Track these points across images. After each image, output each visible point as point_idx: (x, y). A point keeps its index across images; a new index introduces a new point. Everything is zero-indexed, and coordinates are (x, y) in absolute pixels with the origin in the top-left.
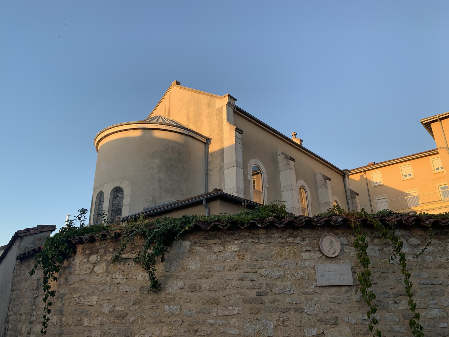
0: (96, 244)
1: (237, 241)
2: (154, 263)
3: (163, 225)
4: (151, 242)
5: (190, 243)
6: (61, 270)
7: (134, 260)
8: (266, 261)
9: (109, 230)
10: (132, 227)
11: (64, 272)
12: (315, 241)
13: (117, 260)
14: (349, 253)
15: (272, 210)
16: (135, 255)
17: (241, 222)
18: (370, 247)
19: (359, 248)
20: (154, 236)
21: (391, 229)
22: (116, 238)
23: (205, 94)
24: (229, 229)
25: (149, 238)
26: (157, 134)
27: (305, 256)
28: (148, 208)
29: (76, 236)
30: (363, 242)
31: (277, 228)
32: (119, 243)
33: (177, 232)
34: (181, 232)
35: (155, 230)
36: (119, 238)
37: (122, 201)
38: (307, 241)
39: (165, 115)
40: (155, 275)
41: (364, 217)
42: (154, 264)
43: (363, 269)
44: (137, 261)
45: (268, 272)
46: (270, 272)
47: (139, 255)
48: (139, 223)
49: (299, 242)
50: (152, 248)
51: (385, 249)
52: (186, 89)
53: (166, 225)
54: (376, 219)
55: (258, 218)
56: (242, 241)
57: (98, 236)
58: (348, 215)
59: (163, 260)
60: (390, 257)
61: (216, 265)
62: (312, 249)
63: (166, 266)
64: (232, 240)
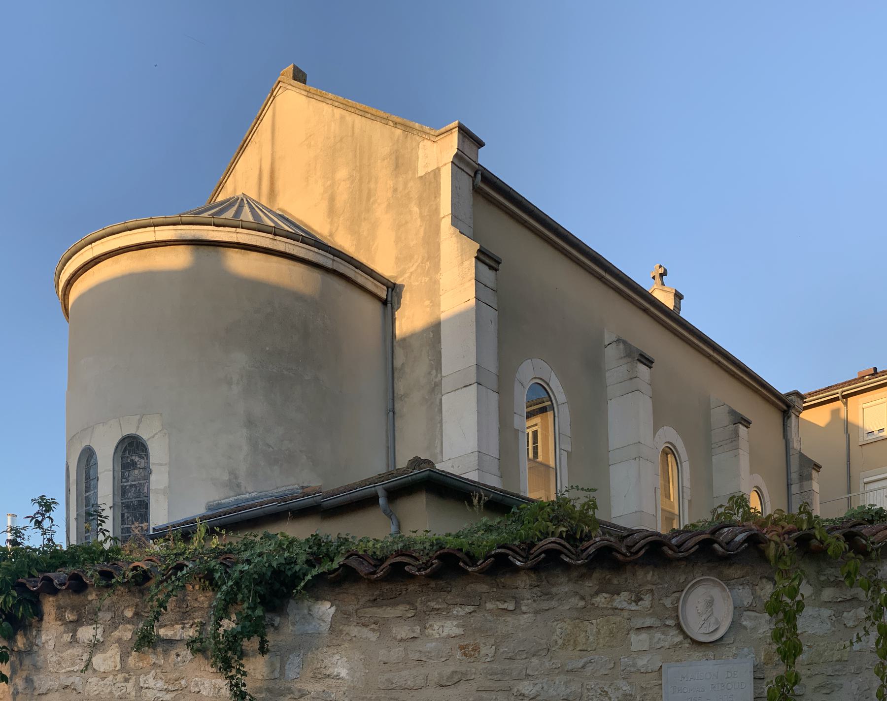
0: (90, 598)
1: (458, 608)
2: (242, 655)
3: (260, 555)
4: (230, 601)
5: (333, 609)
6: (12, 658)
7: (190, 643)
8: (535, 661)
9: (118, 560)
10: (176, 555)
11: (21, 664)
12: (668, 602)
13: (146, 641)
14: (754, 629)
15: (556, 517)
16: (191, 633)
17: (467, 554)
18: (808, 611)
19: (781, 615)
20: (237, 583)
21: (871, 560)
22: (137, 584)
23: (385, 121)
24: (435, 575)
25: (224, 588)
26: (241, 264)
27: (639, 641)
28: (219, 506)
29: (35, 572)
30: (792, 598)
31: (567, 567)
32: (147, 598)
33: (297, 578)
34: (309, 577)
35: (240, 567)
36: (147, 584)
37: (147, 478)
38: (646, 602)
39: (259, 195)
40: (244, 685)
41: (805, 527)
42: (240, 658)
43: (782, 669)
44: (197, 647)
45: (538, 687)
46: (546, 687)
47: (200, 633)
48: (194, 545)
49: (625, 605)
50: (234, 617)
51: (845, 614)
52: (324, 99)
53: (269, 555)
54: (837, 534)
55: (517, 543)
56: (471, 608)
57: (92, 576)
58: (763, 524)
59: (263, 650)
60: (855, 635)
61: (405, 673)
62: (658, 623)
63: (272, 664)
64: (445, 606)
